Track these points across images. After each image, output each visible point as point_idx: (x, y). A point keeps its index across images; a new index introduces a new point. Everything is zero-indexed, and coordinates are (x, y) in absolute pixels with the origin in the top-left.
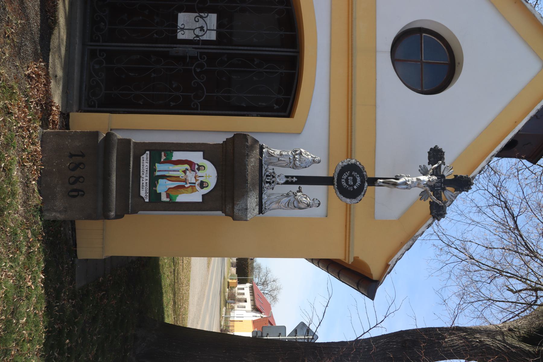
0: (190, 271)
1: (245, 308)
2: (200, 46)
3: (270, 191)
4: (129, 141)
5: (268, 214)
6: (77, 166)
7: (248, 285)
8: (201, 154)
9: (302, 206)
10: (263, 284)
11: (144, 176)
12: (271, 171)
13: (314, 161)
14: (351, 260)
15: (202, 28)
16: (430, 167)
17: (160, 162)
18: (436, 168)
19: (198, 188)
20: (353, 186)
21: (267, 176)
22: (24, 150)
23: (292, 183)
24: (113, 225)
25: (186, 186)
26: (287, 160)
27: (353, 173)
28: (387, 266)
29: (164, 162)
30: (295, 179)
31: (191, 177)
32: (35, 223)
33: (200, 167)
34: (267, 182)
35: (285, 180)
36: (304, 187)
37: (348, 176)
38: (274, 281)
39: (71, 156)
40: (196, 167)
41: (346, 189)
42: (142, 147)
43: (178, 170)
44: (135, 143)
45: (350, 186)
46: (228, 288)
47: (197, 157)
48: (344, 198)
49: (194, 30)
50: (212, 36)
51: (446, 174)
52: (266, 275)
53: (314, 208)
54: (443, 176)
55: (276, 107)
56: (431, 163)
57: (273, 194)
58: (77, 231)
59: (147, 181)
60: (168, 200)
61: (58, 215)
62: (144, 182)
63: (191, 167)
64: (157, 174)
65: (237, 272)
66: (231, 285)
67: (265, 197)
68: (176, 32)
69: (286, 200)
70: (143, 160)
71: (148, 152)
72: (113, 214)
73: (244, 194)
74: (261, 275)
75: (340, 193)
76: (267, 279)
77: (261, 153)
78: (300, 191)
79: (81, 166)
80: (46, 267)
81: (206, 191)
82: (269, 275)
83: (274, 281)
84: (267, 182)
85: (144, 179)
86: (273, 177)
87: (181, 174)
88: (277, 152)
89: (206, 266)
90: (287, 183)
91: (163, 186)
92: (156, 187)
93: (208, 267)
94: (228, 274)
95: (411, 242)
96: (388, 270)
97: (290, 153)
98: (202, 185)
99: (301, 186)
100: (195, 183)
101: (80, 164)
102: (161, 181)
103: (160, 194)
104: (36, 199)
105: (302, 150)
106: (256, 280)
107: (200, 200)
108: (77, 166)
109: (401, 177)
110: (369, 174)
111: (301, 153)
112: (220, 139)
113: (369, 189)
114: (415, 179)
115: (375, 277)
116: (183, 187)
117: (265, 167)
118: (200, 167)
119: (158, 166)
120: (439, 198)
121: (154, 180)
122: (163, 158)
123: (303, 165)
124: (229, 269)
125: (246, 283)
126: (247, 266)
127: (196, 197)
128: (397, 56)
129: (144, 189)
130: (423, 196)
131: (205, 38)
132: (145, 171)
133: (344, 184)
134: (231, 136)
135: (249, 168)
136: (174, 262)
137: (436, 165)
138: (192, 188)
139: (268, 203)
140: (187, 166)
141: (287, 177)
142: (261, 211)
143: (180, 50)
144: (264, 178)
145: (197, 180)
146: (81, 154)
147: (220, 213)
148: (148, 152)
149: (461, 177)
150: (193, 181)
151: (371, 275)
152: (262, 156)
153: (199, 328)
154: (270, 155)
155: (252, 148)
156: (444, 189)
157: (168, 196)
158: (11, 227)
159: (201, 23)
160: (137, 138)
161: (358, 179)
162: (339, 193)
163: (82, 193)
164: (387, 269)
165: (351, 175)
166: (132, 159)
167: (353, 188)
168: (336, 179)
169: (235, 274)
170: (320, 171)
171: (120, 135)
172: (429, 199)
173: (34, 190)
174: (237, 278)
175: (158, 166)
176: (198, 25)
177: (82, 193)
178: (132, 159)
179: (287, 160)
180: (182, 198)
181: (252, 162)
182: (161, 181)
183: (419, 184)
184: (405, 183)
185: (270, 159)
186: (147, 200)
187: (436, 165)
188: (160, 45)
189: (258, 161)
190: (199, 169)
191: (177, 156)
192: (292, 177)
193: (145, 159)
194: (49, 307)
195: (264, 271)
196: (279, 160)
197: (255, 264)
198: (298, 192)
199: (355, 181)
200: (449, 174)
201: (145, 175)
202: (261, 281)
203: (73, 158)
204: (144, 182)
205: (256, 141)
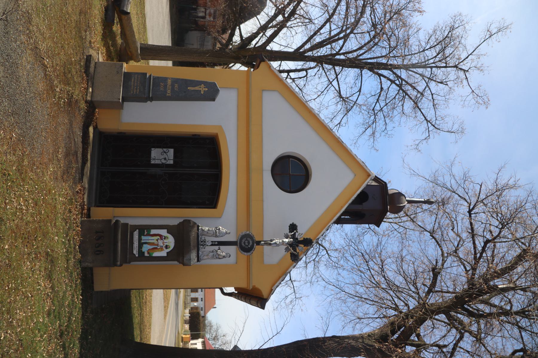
0: (151, 318)
2: (164, 169)
3: (203, 250)
4: (127, 224)
5: (202, 262)
7: (200, 340)
8: (166, 230)
9: (220, 257)
10: (214, 339)
11: (135, 243)
12: (204, 239)
13: (226, 233)
14: (251, 288)
15: (165, 159)
16: (290, 234)
17: (144, 235)
19: (164, 248)
20: (248, 246)
21: (202, 241)
22: (74, 230)
23: (215, 245)
24: (115, 270)
25: (158, 248)
26: (212, 233)
27: (248, 239)
28: (272, 290)
29: (147, 235)
30: (216, 243)
31: (160, 243)
32: (78, 268)
33: (165, 238)
34: (202, 245)
35: (211, 243)
36: (221, 247)
38: (224, 336)
40: (164, 237)
42: (134, 228)
43: (154, 240)
44: (131, 225)
45: (246, 246)
46: (182, 342)
47: (164, 232)
49: (161, 160)
50: (172, 162)
51: (299, 237)
52: (217, 331)
53: (227, 259)
54: (297, 239)
55: (207, 202)
56: (290, 232)
57: (204, 251)
58: (94, 275)
60: (148, 255)
61: (89, 264)
62: (136, 246)
63: (160, 237)
64: (143, 241)
65: (190, 328)
66: (184, 340)
67: (200, 253)
68: (150, 161)
69: (211, 254)
71: (137, 230)
72: (119, 263)
73: (189, 251)
74: (212, 331)
75: (241, 250)
76: (218, 334)
77: (198, 229)
78: (219, 249)
80: (82, 293)
81: (168, 250)
82: (219, 331)
83: (224, 336)
84: (202, 245)
86: (205, 242)
87: (155, 242)
88: (207, 229)
89: (163, 313)
90: (212, 245)
91: (146, 248)
92: (142, 248)
93: (165, 318)
94: (182, 330)
95: (284, 276)
96: (272, 292)
97: (213, 229)
98: (167, 247)
99: (220, 246)
102: (144, 245)
103: (144, 252)
104: (79, 256)
105: (220, 227)
106: (208, 336)
107: (165, 255)
109: (274, 240)
110: (257, 239)
111: (219, 229)
112: (175, 222)
113: (257, 247)
114: (281, 241)
115: (265, 297)
116: (156, 248)
117: (200, 237)
118: (165, 238)
119: (143, 237)
120: (295, 250)
121: (141, 245)
122: (146, 233)
123: (221, 235)
124: (183, 326)
125: (198, 339)
126: (199, 323)
127: (164, 254)
130: (287, 250)
131: (168, 163)
133: (243, 244)
134: (181, 220)
135: (192, 237)
136: (140, 307)
137: (293, 233)
138: (161, 249)
139: (202, 256)
140: (158, 237)
141: (212, 242)
142: (198, 261)
143: (153, 171)
144: (200, 242)
145: (164, 245)
147: (176, 262)
148: (137, 230)
149: (307, 238)
150: (162, 245)
151: (263, 296)
152: (198, 231)
153: (163, 345)
154: (203, 230)
155: (193, 227)
156: (298, 246)
157: (148, 253)
158: (71, 270)
159: (165, 156)
160: (132, 222)
161: (251, 242)
164: (271, 292)
165: (246, 240)
166: (129, 234)
169: (188, 330)
170: (232, 238)
171: (122, 221)
172: (290, 252)
173: (77, 251)
174: (190, 333)
175: (143, 237)
176: (163, 157)
178: (129, 234)
179: (212, 233)
180: (156, 254)
181: (193, 234)
182: (144, 245)
183: (283, 243)
184: (276, 243)
186: (137, 256)
187: (293, 233)
188: (141, 168)
189: (196, 234)
190: (165, 239)
191: (153, 232)
192: (215, 242)
194: (83, 315)
195: (215, 327)
196: (208, 233)
197: (206, 322)
198: (219, 249)
199: (249, 243)
200: (300, 238)
202: (212, 337)
204: (136, 246)
205: (195, 223)
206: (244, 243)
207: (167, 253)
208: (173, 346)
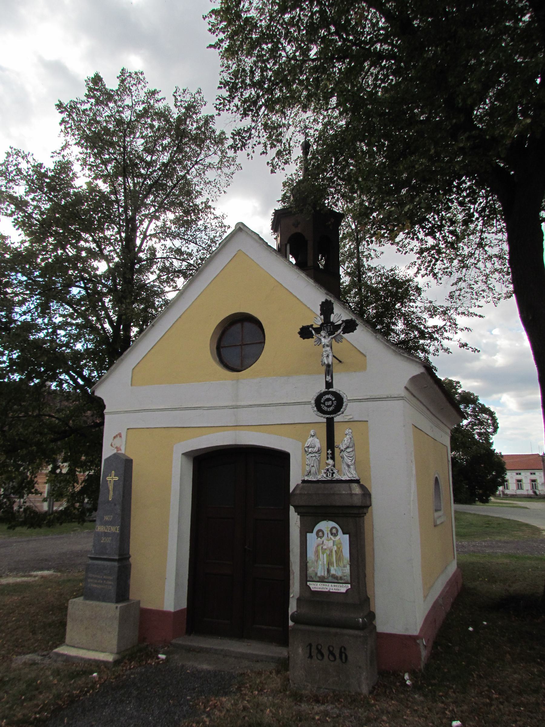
6: (320, 652)
8: (308, 534)
18: (316, 332)
20: (332, 401)
21: (327, 476)
27: (322, 401)
37: (325, 405)
41: (336, 407)
45: (333, 403)
51: (320, 323)
54: (322, 325)
56: (311, 336)
62: (334, 588)
71: (308, 583)
75: (339, 411)
84: (332, 476)
85: (331, 588)
90: (333, 458)
100: (334, 542)
101: (317, 648)
107: (347, 536)
108: (320, 652)
128: (239, 368)
129: (340, 588)
132: (324, 587)
133: (331, 409)
137: (313, 332)
144: (328, 479)
146: (309, 647)
161: (327, 396)
165: (324, 404)
167: (335, 400)
187: (313, 332)
192: (328, 454)
199: (328, 400)
201: (326, 587)
203: (313, 654)
206: (329, 406)
207: (344, 533)
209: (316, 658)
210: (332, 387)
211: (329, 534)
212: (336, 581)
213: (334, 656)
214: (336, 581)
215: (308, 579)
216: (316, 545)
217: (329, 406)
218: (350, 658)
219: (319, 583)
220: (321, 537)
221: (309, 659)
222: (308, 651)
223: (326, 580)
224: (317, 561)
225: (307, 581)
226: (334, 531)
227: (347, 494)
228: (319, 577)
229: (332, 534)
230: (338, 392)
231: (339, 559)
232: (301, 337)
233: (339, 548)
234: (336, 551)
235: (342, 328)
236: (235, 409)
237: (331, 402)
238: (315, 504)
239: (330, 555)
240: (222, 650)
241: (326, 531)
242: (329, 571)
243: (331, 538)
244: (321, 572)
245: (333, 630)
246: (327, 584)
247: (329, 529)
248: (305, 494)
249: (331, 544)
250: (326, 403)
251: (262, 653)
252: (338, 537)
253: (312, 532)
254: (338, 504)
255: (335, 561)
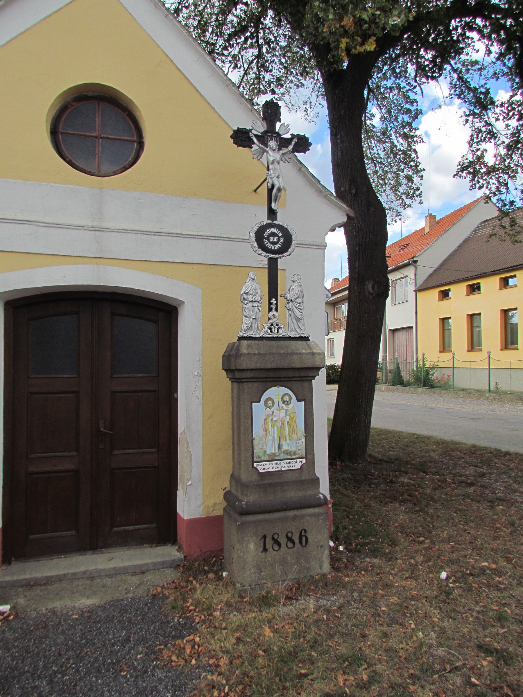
1: (465, 345)
34: (278, 332)
37: (269, 241)
39: (265, 550)
45: (279, 240)
48: (292, 247)
59: (285, 463)
62: (286, 465)
70: (264, 469)
71: (255, 465)
79: (276, 537)
85: (283, 466)
100: (286, 411)
101: (273, 538)
129: (293, 464)
132: (275, 466)
133: (277, 247)
141: (270, 310)
146: (263, 540)
161: (272, 230)
162: (286, 254)
163: (303, 532)
165: (268, 239)
167: (281, 236)
168: (272, 256)
177: (303, 532)
185: (254, 328)
193: (262, 467)
199: (273, 235)
201: (278, 466)
203: (267, 547)
206: (274, 243)
207: (298, 400)
208: (371, 426)
209: (271, 549)
210: (276, 220)
211: (281, 403)
212: (289, 457)
213: (293, 542)
214: (289, 457)
215: (255, 459)
216: (264, 417)
217: (274, 243)
218: (310, 540)
219: (268, 463)
220: (270, 407)
221: (263, 554)
222: (262, 545)
223: (277, 458)
224: (266, 437)
225: (253, 462)
226: (286, 398)
227: (308, 353)
228: (269, 455)
229: (284, 402)
230: (286, 227)
231: (292, 432)
232: (235, 143)
233: (292, 419)
234: (288, 422)
235: (293, 143)
236: (97, 233)
237: (277, 238)
238: (269, 366)
239: (282, 427)
240: (84, 573)
241: (277, 400)
242: (280, 446)
243: (282, 407)
244: (272, 449)
245: (291, 513)
246: (279, 462)
247: (281, 397)
248: (255, 354)
249: (282, 414)
250: (270, 238)
251: (149, 561)
252: (291, 406)
253: (259, 402)
254: (298, 365)
255: (287, 434)
